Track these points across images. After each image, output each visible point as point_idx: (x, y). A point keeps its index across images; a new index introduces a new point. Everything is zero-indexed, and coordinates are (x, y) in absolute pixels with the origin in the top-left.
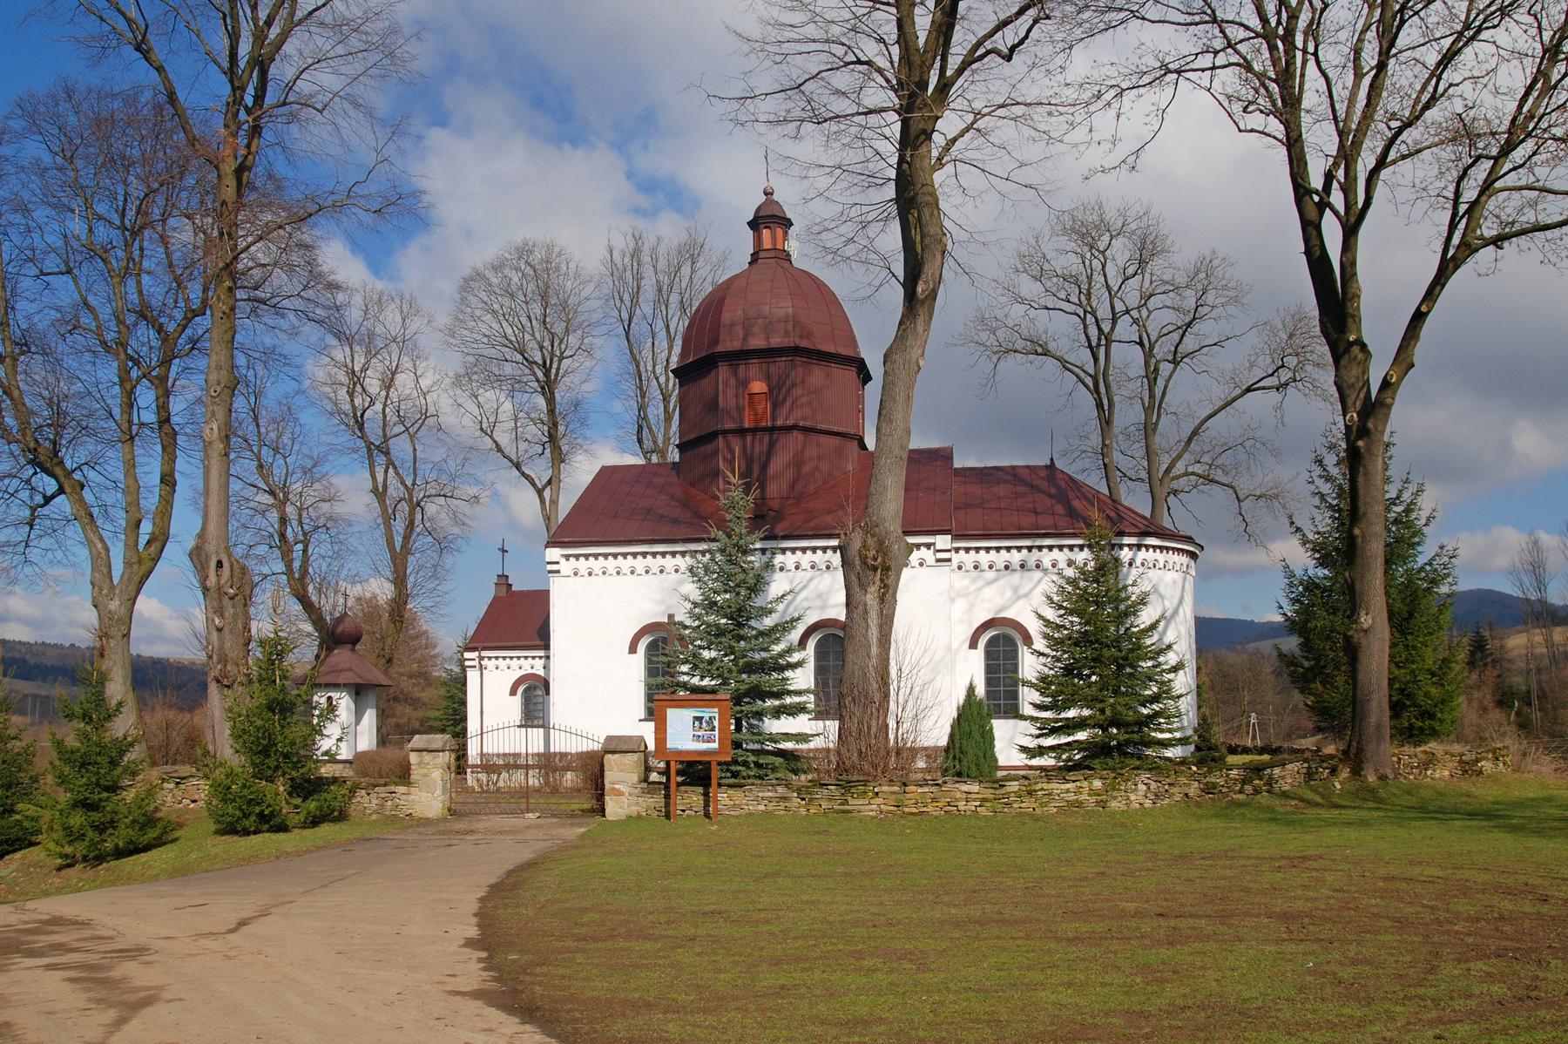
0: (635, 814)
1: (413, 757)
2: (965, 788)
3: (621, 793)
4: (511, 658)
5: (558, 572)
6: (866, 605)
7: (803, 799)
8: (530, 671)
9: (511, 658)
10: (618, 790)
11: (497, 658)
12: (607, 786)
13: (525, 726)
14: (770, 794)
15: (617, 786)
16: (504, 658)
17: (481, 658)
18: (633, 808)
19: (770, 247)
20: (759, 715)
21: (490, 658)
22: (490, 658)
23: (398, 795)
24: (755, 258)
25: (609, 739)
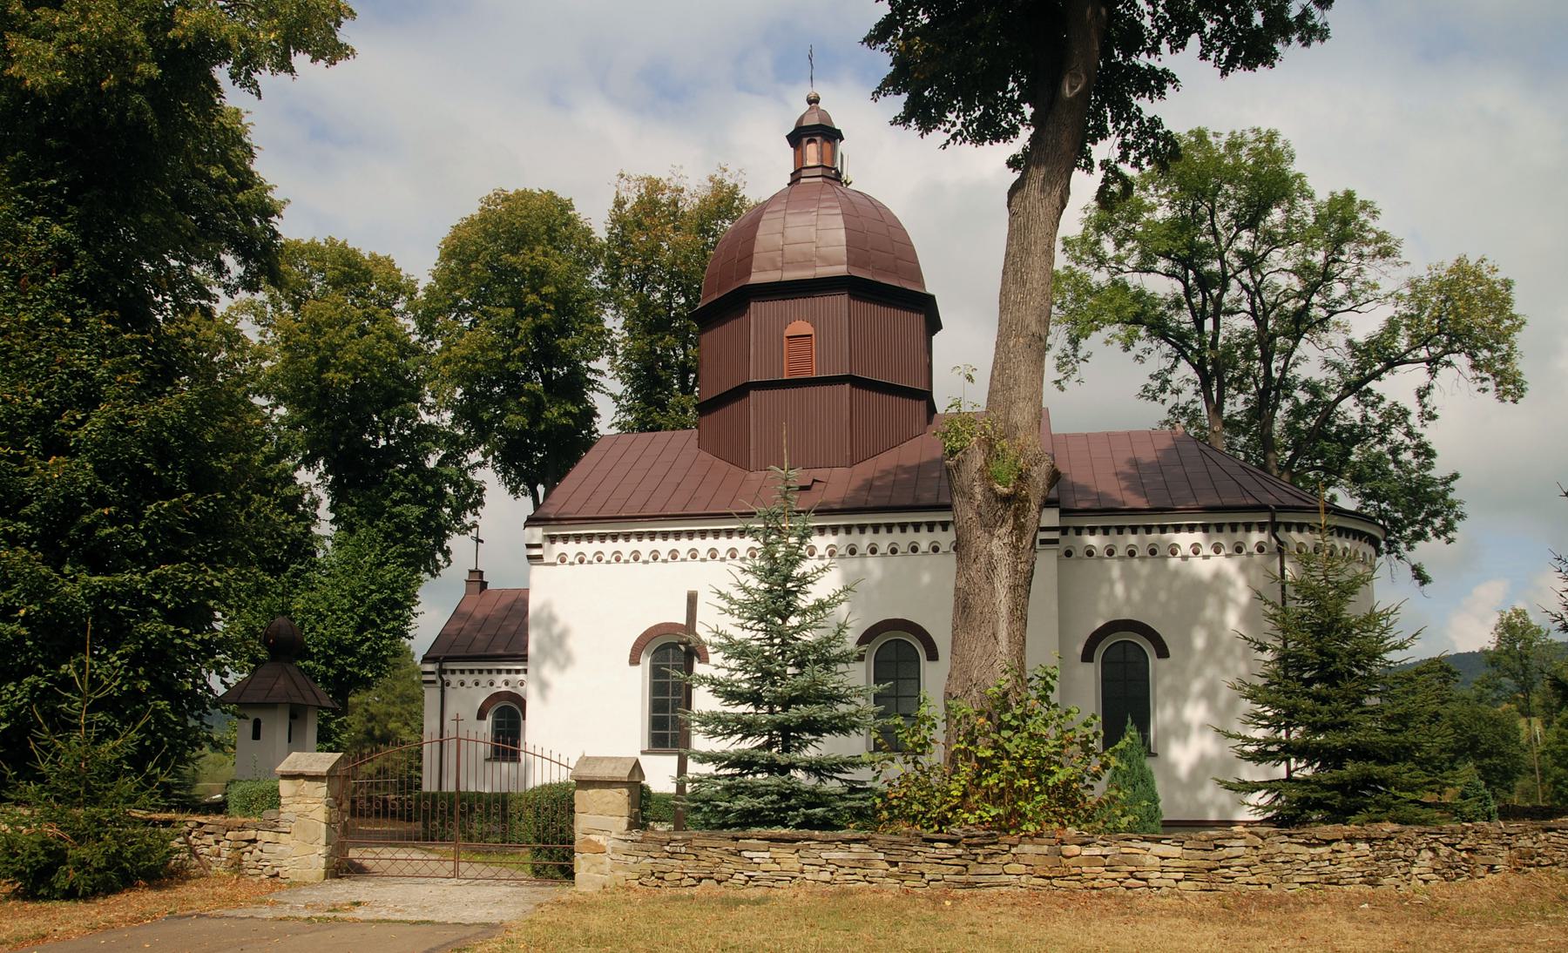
0: (622, 883)
1: (285, 787)
2: (1158, 849)
3: (601, 850)
4: (481, 671)
5: (540, 557)
6: (991, 556)
7: (896, 864)
8: (504, 688)
9: (481, 671)
10: (596, 844)
11: (462, 672)
12: (578, 836)
13: (496, 759)
14: (840, 855)
15: (593, 837)
16: (472, 672)
17: (442, 672)
18: (620, 873)
19: (814, 164)
20: (1079, 531)
21: (453, 672)
22: (453, 672)
23: (259, 845)
24: (796, 177)
25: (585, 761)
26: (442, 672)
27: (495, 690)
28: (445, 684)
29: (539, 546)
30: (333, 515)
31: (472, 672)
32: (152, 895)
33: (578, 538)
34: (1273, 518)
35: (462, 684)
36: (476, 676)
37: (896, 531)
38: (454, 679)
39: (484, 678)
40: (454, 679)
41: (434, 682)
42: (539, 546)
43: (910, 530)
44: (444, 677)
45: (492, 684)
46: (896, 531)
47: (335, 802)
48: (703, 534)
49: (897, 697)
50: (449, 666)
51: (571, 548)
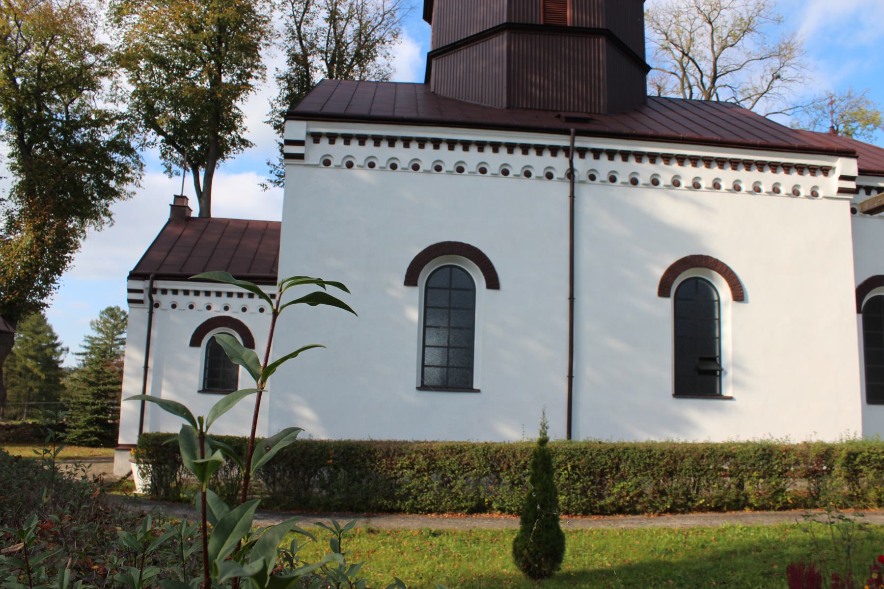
4: (197, 293)
5: (301, 157)
9: (197, 293)
11: (175, 292)
16: (186, 292)
17: (153, 291)
21: (164, 291)
22: (164, 291)
26: (153, 291)
27: (212, 314)
28: (154, 305)
29: (301, 143)
30: (286, 108)
31: (186, 292)
32: (675, 440)
33: (653, 158)
34: (573, 142)
35: (191, 307)
36: (192, 298)
37: (444, 147)
38: (165, 300)
39: (201, 301)
40: (165, 300)
41: (141, 302)
42: (301, 143)
43: (414, 146)
44: (154, 297)
45: (209, 308)
46: (399, 145)
47: (243, 440)
48: (667, 158)
49: (448, 367)
50: (160, 284)
51: (338, 151)
